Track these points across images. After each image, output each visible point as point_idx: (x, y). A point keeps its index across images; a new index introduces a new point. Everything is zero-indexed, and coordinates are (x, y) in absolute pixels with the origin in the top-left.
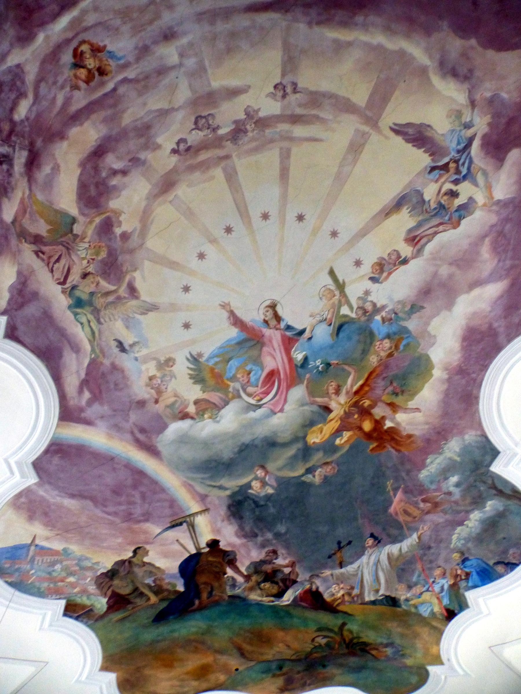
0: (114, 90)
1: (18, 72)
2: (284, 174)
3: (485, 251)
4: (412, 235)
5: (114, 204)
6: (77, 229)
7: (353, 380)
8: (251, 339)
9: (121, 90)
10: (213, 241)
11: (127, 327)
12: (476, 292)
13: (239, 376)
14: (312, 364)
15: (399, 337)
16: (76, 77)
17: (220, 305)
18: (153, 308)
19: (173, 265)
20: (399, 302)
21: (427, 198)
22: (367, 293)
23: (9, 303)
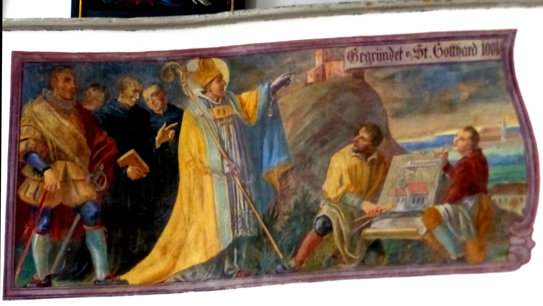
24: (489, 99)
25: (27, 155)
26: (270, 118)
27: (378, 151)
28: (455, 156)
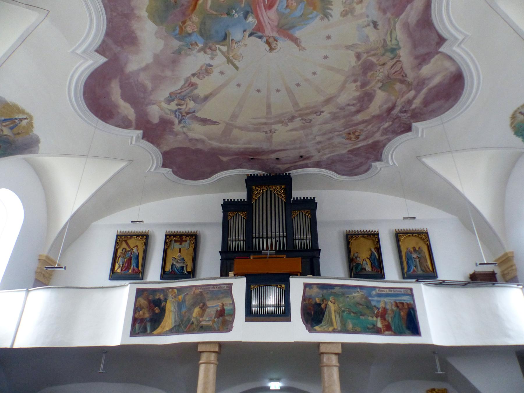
0: (345, 129)
1: (383, 134)
2: (269, 107)
3: (149, 85)
4: (194, 87)
5: (357, 94)
6: (380, 84)
7: (207, 3)
8: (286, 30)
9: (343, 129)
10: (307, 80)
11: (368, 37)
12: (143, 65)
13: (295, 4)
14: (241, 14)
15: (182, 35)
16: (360, 133)
17: (305, 49)
18: (347, 47)
19: (331, 69)
20: (189, 55)
21: (192, 102)
22: (212, 58)
23: (434, 56)
24: (227, 297)
25: (137, 308)
26: (184, 301)
27: (204, 308)
28: (219, 309)
